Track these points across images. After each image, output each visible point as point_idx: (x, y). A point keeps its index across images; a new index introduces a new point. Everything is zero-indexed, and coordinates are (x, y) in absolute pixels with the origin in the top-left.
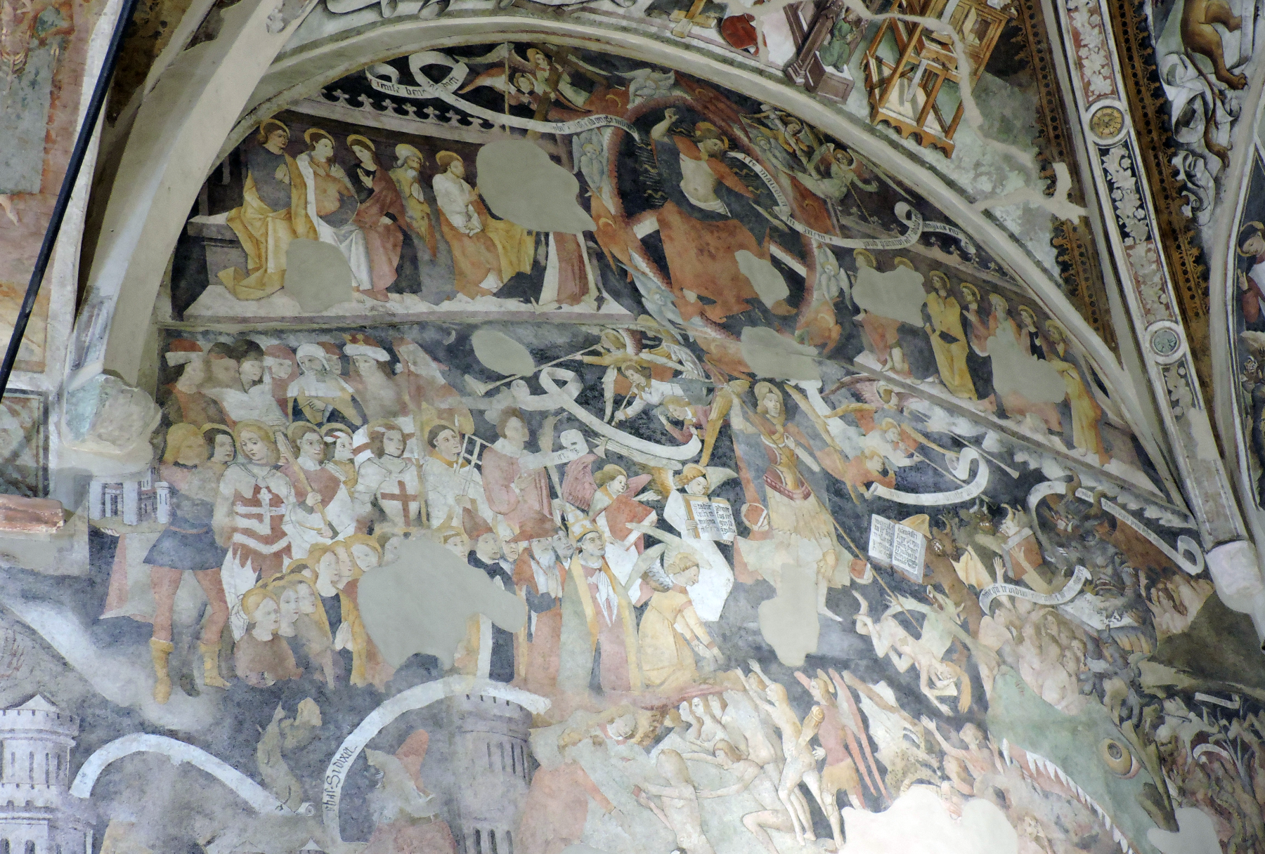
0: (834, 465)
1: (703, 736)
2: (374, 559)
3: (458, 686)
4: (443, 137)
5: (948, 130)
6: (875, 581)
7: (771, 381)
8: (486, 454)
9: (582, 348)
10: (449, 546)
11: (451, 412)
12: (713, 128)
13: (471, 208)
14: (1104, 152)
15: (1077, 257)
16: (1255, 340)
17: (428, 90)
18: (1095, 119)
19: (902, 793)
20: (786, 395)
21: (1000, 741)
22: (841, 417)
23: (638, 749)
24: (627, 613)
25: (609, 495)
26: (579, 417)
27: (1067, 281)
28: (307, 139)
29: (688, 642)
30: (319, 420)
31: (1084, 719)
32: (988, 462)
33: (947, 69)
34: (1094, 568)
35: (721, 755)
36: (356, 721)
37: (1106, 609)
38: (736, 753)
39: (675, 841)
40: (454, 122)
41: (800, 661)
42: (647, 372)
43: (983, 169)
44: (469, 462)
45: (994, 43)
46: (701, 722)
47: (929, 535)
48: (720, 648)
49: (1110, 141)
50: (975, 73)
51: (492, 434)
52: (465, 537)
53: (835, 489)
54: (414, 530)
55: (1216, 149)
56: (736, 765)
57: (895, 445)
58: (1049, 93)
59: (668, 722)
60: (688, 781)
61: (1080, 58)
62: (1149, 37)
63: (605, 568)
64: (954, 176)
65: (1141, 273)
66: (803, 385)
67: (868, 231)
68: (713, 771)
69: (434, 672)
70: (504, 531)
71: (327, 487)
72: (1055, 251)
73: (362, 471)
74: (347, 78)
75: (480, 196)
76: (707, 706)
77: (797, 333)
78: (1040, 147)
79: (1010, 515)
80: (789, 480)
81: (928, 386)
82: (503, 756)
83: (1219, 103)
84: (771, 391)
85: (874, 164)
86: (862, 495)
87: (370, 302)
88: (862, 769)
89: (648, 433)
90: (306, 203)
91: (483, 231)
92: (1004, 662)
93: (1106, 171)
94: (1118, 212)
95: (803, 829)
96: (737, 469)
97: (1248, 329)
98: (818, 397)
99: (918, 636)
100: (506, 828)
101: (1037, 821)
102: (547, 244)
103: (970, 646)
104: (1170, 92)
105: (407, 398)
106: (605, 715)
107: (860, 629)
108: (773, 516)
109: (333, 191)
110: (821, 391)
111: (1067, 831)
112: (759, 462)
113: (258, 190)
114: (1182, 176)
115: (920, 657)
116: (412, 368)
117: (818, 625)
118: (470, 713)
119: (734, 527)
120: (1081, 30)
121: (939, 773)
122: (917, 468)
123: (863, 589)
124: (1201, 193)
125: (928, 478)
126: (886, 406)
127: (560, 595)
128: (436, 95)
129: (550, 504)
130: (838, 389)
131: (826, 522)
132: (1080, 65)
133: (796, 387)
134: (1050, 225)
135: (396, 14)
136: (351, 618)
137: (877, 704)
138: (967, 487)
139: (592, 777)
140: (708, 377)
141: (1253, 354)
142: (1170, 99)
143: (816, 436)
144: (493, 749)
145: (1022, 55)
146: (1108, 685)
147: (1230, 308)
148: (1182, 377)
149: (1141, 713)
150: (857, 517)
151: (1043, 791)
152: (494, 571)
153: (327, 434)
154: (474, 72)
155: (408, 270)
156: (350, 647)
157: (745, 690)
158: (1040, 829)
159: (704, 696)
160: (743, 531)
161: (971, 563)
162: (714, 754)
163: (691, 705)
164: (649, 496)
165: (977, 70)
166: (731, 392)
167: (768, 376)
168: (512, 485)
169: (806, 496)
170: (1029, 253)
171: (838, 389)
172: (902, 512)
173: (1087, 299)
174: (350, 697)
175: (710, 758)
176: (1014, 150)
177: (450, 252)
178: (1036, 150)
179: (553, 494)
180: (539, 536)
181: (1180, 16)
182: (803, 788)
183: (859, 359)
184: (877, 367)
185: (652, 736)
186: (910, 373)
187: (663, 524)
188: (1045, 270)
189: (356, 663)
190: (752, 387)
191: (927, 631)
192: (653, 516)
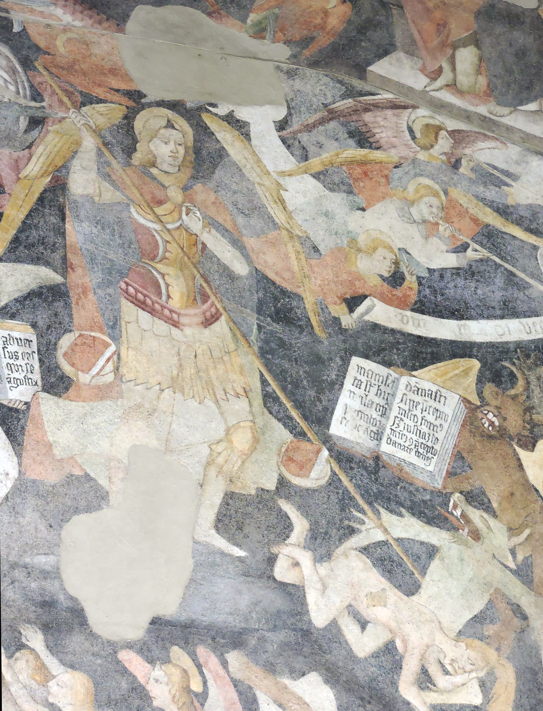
0: (281, 264)
6: (334, 481)
7: (175, 106)
20: (202, 131)
22: (316, 176)
41: (135, 629)
53: (277, 306)
57: (430, 228)
66: (243, 113)
77: (253, 17)
80: (176, 289)
84: (170, 125)
86: (336, 321)
96: (65, 267)
98: (273, 138)
99: (411, 589)
103: (529, 610)
107: (282, 572)
108: (128, 355)
110: (281, 126)
112: (116, 256)
115: (408, 629)
117: (191, 562)
119: (37, 376)
122: (470, 272)
123: (304, 498)
125: (494, 292)
126: (422, 156)
130: (322, 122)
131: (246, 368)
140: (37, 96)
143: (255, 209)
160: (56, 383)
166: (79, 131)
167: (169, 97)
169: (209, 321)
171: (322, 122)
172: (422, 353)
183: (380, 68)
184: (419, 82)
186: (490, 92)
190: (129, 118)
191: (434, 579)
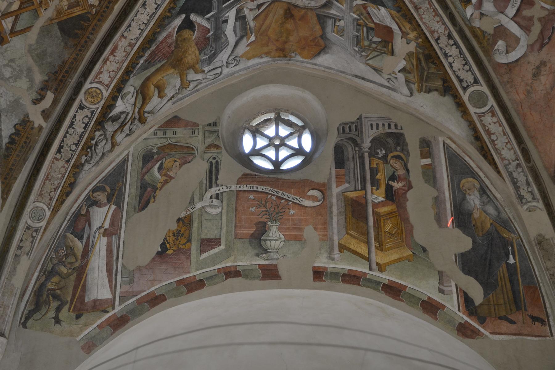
5: (14, 32)
14: (81, 107)
15: (22, 142)
16: (72, 241)
18: (90, 90)
33: (41, 6)
43: (13, 64)
45: (73, 15)
49: (88, 105)
50: (52, 20)
55: (114, 141)
58: (75, 59)
61: (108, 59)
62: (132, 72)
65: (52, 174)
78: (49, 79)
83: (130, 123)
93: (75, 116)
94: (65, 139)
97: (72, 233)
104: (119, 102)
114: (93, 142)
120: (119, 47)
124: (94, 155)
132: (105, 62)
134: (22, 117)
141: (67, 247)
142: (117, 105)
145: (79, 32)
147: (68, 217)
148: (32, 237)
165: (54, 19)
173: (10, 165)
176: (36, 69)
178: (46, 78)
181: (149, 74)
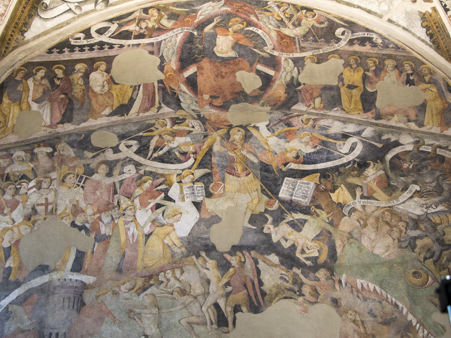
1: (169, 286)
2: (29, 230)
3: (55, 276)
4: (100, 56)
8: (88, 182)
9: (144, 130)
10: (64, 221)
11: (75, 167)
12: (240, 20)
13: (105, 82)
15: (436, 29)
17: (97, 38)
19: (273, 304)
21: (341, 275)
23: (133, 294)
24: (141, 238)
25: (142, 189)
26: (134, 159)
27: (433, 42)
28: (34, 71)
29: (169, 247)
30: (16, 179)
31: (399, 260)
32: (363, 142)
34: (424, 183)
35: (176, 294)
36: (7, 294)
37: (426, 204)
38: (183, 292)
39: (143, 332)
40: (106, 49)
42: (174, 134)
44: (78, 185)
46: (168, 280)
47: (318, 183)
48: (186, 248)
51: (90, 172)
52: (71, 216)
54: (49, 217)
56: (182, 298)
59: (152, 282)
60: (156, 306)
63: (135, 219)
64: (369, 8)
66: (257, 125)
67: (316, 46)
68: (170, 301)
69: (46, 272)
70: (90, 211)
71: (14, 205)
72: (425, 30)
73: (30, 197)
74: (60, 43)
75: (111, 77)
76: (173, 273)
77: (261, 102)
79: (372, 166)
81: (336, 112)
82: (69, 302)
84: (239, 131)
85: (328, 14)
86: (281, 169)
87: (49, 130)
88: (252, 294)
89: (167, 160)
90: (28, 96)
91: (109, 91)
92: (352, 237)
95: (212, 323)
100: (64, 331)
101: (356, 312)
102: (139, 90)
105: (56, 165)
106: (122, 281)
107: (265, 231)
109: (41, 90)
111: (375, 316)
113: (8, 96)
116: (61, 153)
118: (59, 286)
121: (298, 293)
126: (305, 126)
127: (111, 234)
128: (100, 40)
129: (113, 197)
133: (255, 127)
134: (419, 17)
135: (83, 12)
136: (15, 254)
137: (268, 264)
138: (346, 156)
139: (109, 308)
144: (66, 300)
146: (419, 243)
149: (441, 254)
150: (276, 180)
151: (363, 297)
152: (81, 228)
153: (18, 185)
154: (120, 26)
155: (68, 113)
156: (12, 265)
157: (195, 264)
158: (357, 316)
159: (173, 269)
160: (209, 195)
161: (341, 192)
162: (172, 294)
163: (165, 274)
164: (163, 187)
168: (97, 192)
169: (247, 175)
170: (414, 35)
173: (445, 49)
174: (7, 285)
175: (169, 295)
177: (90, 103)
179: (115, 192)
180: (105, 211)
182: (216, 306)
185: (142, 288)
187: (167, 198)
188: (423, 41)
189: (13, 271)
192: (163, 195)
